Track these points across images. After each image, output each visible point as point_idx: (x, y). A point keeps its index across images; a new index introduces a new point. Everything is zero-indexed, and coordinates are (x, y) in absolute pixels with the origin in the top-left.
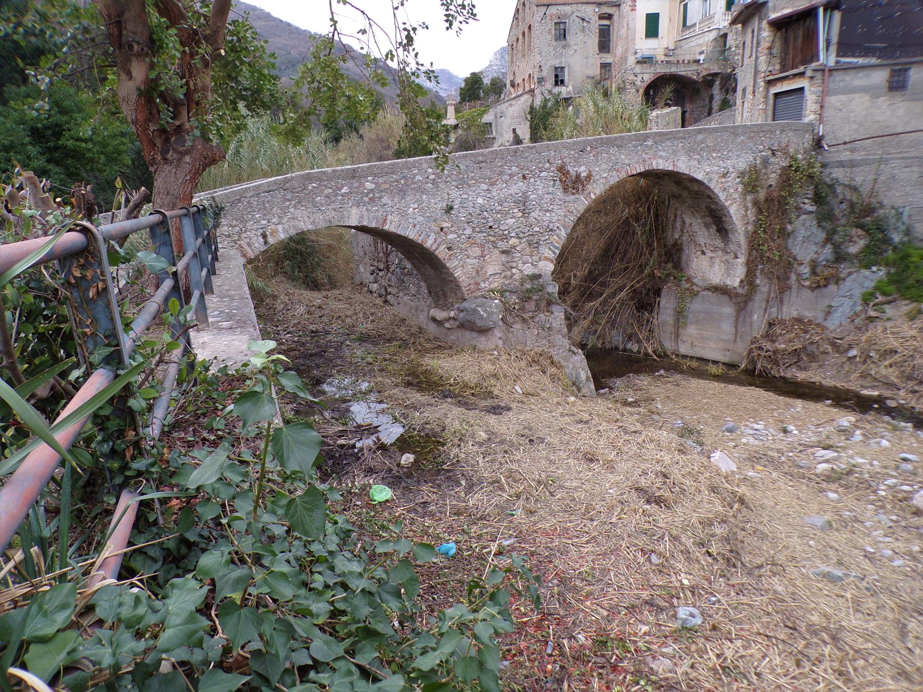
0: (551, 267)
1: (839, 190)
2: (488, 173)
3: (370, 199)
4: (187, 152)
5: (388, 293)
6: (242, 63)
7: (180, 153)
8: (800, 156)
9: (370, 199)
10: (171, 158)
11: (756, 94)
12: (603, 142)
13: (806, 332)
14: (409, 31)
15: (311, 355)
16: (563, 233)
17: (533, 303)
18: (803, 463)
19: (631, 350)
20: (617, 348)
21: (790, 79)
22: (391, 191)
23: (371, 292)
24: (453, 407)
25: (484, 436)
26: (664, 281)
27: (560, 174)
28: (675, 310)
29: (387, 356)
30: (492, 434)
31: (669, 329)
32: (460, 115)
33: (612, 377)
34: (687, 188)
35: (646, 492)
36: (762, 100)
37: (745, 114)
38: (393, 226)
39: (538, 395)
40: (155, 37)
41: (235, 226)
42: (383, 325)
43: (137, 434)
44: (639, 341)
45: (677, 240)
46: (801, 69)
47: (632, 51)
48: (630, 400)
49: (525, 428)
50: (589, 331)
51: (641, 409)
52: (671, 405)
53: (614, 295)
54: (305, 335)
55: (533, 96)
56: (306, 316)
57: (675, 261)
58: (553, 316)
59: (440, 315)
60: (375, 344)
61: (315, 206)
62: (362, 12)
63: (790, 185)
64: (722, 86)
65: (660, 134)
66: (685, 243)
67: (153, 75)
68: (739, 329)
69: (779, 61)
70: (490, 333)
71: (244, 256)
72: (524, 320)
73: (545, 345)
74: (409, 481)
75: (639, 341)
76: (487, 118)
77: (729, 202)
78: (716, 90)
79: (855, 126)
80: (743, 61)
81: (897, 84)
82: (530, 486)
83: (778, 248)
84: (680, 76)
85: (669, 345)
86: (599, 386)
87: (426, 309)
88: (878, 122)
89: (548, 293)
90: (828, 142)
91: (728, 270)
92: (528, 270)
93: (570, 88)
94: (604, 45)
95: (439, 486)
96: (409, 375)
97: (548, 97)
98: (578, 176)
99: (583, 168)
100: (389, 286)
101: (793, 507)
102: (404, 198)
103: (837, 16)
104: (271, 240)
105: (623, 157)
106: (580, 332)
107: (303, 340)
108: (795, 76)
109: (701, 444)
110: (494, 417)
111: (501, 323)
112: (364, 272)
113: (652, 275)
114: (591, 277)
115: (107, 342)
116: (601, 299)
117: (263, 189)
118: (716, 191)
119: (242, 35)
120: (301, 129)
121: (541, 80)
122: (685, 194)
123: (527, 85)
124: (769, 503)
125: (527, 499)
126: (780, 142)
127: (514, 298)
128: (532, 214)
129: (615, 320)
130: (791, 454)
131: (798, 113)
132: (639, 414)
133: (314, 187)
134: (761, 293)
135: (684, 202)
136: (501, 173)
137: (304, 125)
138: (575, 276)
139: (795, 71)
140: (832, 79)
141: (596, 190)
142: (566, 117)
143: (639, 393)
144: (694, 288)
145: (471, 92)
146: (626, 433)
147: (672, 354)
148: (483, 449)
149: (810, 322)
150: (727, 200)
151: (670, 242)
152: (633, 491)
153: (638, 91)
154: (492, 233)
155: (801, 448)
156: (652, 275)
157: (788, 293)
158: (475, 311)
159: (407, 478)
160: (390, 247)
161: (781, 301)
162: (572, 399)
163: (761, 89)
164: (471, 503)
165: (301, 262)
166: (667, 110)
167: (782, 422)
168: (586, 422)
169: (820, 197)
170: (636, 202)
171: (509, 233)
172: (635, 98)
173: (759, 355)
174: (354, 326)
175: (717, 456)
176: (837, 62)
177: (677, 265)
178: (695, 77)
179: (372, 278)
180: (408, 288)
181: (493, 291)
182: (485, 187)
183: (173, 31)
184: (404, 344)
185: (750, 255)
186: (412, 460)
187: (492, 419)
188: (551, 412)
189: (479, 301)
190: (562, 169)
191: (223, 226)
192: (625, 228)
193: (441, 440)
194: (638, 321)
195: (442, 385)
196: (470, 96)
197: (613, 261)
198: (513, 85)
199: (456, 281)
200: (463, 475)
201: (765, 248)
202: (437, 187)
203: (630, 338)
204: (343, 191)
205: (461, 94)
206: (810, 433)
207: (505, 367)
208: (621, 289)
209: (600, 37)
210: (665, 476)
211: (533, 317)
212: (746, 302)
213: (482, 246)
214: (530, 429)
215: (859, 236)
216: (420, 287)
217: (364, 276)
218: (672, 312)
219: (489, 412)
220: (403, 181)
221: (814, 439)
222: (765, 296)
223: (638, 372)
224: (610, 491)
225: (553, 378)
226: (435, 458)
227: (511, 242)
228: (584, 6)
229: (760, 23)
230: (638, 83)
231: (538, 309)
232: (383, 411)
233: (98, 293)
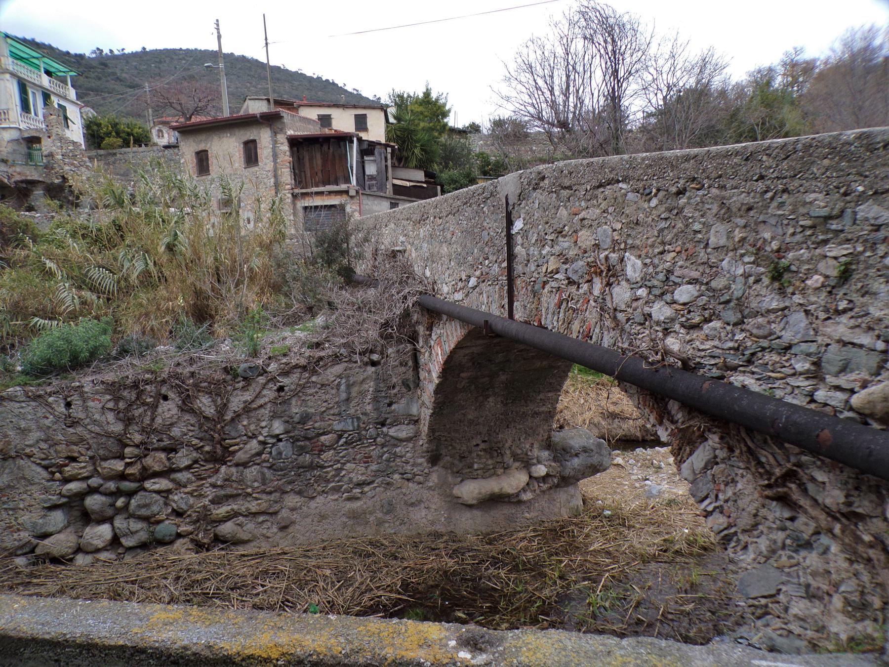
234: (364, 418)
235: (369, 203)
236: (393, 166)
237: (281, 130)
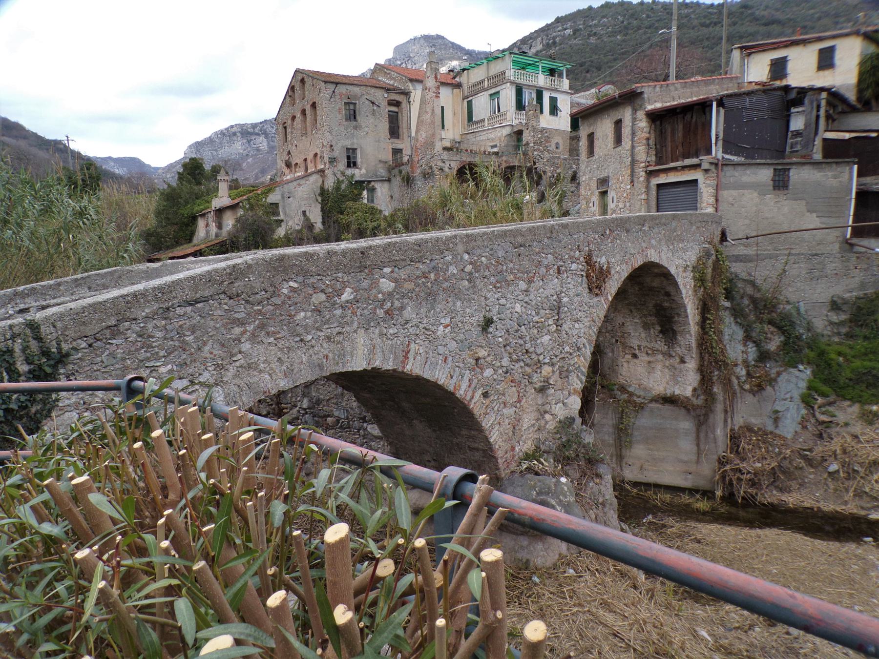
1: (740, 285)
2: (526, 263)
3: (386, 312)
11: (636, 184)
21: (680, 171)
36: (644, 190)
68: (702, 447)
79: (747, 222)
81: (781, 183)
88: (767, 218)
94: (394, 131)
97: (341, 179)
117: (180, 295)
131: (694, 205)
139: (688, 162)
144: (635, 398)
163: (642, 179)
191: (64, 410)
202: (474, 287)
212: (706, 415)
215: (772, 333)
218: (611, 430)
228: (373, 90)
230: (446, 169)
234: (351, 412)
235: (737, 174)
236: (828, 117)
237: (641, 106)
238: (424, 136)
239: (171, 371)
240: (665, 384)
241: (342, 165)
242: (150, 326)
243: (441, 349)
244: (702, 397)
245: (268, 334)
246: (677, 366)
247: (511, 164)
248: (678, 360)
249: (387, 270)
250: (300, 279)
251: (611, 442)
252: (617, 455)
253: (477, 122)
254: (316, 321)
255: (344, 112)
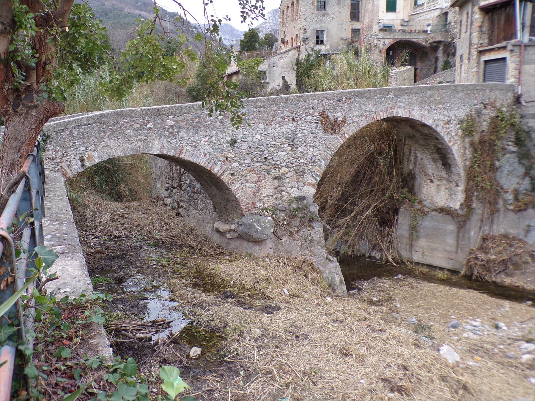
0: (313, 191)
2: (265, 115)
4: (35, 107)
5: (180, 207)
6: (80, 34)
7: (29, 107)
8: (504, 109)
9: (170, 133)
10: (20, 112)
11: (471, 61)
12: (355, 94)
13: (511, 246)
14: (215, 22)
15: (115, 257)
16: (323, 165)
17: (298, 220)
18: (512, 354)
19: (375, 258)
20: (364, 256)
21: (496, 51)
22: (187, 128)
23: (166, 205)
24: (233, 307)
25: (258, 332)
26: (401, 202)
27: (321, 119)
28: (410, 226)
29: (178, 260)
30: (265, 330)
31: (405, 241)
32: (241, 63)
33: (360, 280)
34: (420, 131)
35: (390, 382)
36: (476, 65)
37: (463, 75)
38: (187, 155)
39: (302, 296)
40: (16, 19)
41: (59, 151)
42: (175, 232)
43: (28, 394)
44: (381, 250)
45: (411, 170)
46: (504, 44)
47: (377, 21)
48: (375, 299)
49: (291, 326)
50: (342, 241)
51: (383, 308)
52: (407, 305)
53: (361, 212)
54: (109, 240)
55: (299, 51)
56: (111, 223)
57: (410, 186)
58: (314, 231)
59: (223, 227)
60: (169, 249)
61: (125, 137)
62: (179, 4)
63: (497, 131)
64: (445, 51)
65: (399, 90)
66: (417, 173)
67: (12, 48)
68: (460, 243)
69: (487, 36)
70: (263, 243)
71: (65, 175)
72: (291, 234)
73: (307, 254)
74: (197, 371)
75: (381, 250)
76: (263, 67)
77: (452, 143)
78: (440, 53)
80: (460, 34)
82: (297, 377)
83: (490, 180)
84: (413, 42)
85: (405, 254)
86: (350, 287)
87: (211, 222)
89: (311, 212)
90: (525, 99)
91: (451, 196)
92: (295, 193)
93: (328, 47)
94: (355, 15)
95: (222, 376)
96: (196, 277)
97: (311, 53)
98: (335, 120)
99: (339, 114)
100: (181, 201)
101: (504, 391)
102: (197, 133)
103: (530, 6)
104: (88, 164)
105: (370, 106)
106: (334, 242)
107: (108, 244)
108: (499, 48)
109: (432, 338)
110: (266, 315)
111: (272, 236)
112: (160, 188)
113: (391, 197)
114: (344, 198)
115: (10, 322)
116: (351, 215)
117: (83, 122)
118: (442, 134)
119: (82, 15)
120: (125, 89)
121: (305, 40)
122: (418, 135)
123: (294, 43)
124: (486, 388)
125: (295, 388)
126: (489, 98)
127: (283, 216)
128: (299, 148)
129: (363, 232)
130: (502, 347)
132: (382, 312)
133: (125, 122)
134: (477, 214)
135: (417, 141)
136: (276, 116)
137: (128, 85)
138: (331, 197)
140: (526, 52)
141: (349, 131)
142: (325, 71)
143: (382, 294)
144: (425, 209)
145: (249, 44)
146: (373, 331)
147: (408, 261)
148: (258, 344)
149: (514, 238)
150: (450, 141)
151: (406, 172)
152: (380, 381)
153: (380, 52)
154: (267, 163)
155: (509, 341)
156: (391, 197)
157: (497, 215)
158: (251, 225)
159: (195, 368)
160: (182, 170)
161: (492, 221)
162: (329, 299)
163: (475, 57)
164: (248, 391)
165: (109, 178)
166: (403, 69)
167: (494, 319)
168: (341, 321)
169: (520, 141)
170: (380, 140)
171: (281, 163)
172: (379, 58)
173: (476, 264)
174: (150, 233)
175: (445, 349)
176: (530, 40)
177: (411, 190)
178: (424, 43)
179: (167, 193)
180: (197, 204)
181: (266, 209)
182: (262, 126)
183: (31, 15)
184: (193, 250)
185: (468, 184)
186: (199, 353)
187: (265, 317)
188: (313, 312)
189: (255, 217)
190: (323, 114)
191: (49, 151)
192: (371, 160)
193: (223, 335)
194: (381, 234)
195: (224, 287)
196: (248, 47)
197: (361, 185)
198: (283, 42)
199: (237, 201)
200: (242, 366)
201: (479, 179)
203: (374, 247)
204: (148, 126)
205: (241, 45)
206: (516, 329)
207: (275, 272)
208: (368, 208)
209: (351, 9)
210: (405, 369)
211: (298, 231)
213: (258, 173)
214: (296, 327)
216: (207, 204)
217: (160, 191)
218: (407, 228)
219: (262, 311)
220: (197, 120)
221: (520, 334)
222: (480, 217)
223: (380, 276)
224: (362, 381)
225: (313, 281)
226: (218, 351)
227: (282, 171)
229: (473, 8)
231: (302, 224)
232: (175, 309)
233: (7, 285)
238: (367, 21)
239: (79, 144)
240: (445, 201)
241: (312, 43)
242: (73, 130)
243: (202, 151)
244: (465, 210)
245: (114, 137)
246: (453, 188)
247: (437, 40)
248: (455, 185)
249: (170, 117)
250: (128, 119)
251: (407, 235)
252: (409, 244)
253: (420, 5)
254: (135, 134)
255: (316, 4)
